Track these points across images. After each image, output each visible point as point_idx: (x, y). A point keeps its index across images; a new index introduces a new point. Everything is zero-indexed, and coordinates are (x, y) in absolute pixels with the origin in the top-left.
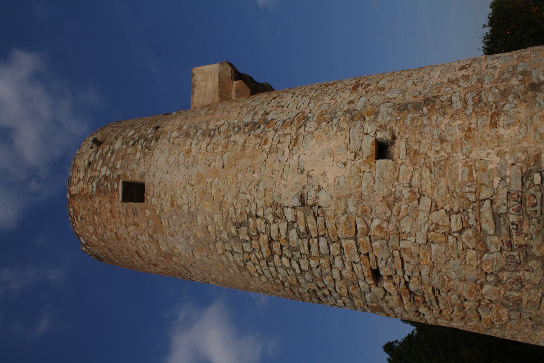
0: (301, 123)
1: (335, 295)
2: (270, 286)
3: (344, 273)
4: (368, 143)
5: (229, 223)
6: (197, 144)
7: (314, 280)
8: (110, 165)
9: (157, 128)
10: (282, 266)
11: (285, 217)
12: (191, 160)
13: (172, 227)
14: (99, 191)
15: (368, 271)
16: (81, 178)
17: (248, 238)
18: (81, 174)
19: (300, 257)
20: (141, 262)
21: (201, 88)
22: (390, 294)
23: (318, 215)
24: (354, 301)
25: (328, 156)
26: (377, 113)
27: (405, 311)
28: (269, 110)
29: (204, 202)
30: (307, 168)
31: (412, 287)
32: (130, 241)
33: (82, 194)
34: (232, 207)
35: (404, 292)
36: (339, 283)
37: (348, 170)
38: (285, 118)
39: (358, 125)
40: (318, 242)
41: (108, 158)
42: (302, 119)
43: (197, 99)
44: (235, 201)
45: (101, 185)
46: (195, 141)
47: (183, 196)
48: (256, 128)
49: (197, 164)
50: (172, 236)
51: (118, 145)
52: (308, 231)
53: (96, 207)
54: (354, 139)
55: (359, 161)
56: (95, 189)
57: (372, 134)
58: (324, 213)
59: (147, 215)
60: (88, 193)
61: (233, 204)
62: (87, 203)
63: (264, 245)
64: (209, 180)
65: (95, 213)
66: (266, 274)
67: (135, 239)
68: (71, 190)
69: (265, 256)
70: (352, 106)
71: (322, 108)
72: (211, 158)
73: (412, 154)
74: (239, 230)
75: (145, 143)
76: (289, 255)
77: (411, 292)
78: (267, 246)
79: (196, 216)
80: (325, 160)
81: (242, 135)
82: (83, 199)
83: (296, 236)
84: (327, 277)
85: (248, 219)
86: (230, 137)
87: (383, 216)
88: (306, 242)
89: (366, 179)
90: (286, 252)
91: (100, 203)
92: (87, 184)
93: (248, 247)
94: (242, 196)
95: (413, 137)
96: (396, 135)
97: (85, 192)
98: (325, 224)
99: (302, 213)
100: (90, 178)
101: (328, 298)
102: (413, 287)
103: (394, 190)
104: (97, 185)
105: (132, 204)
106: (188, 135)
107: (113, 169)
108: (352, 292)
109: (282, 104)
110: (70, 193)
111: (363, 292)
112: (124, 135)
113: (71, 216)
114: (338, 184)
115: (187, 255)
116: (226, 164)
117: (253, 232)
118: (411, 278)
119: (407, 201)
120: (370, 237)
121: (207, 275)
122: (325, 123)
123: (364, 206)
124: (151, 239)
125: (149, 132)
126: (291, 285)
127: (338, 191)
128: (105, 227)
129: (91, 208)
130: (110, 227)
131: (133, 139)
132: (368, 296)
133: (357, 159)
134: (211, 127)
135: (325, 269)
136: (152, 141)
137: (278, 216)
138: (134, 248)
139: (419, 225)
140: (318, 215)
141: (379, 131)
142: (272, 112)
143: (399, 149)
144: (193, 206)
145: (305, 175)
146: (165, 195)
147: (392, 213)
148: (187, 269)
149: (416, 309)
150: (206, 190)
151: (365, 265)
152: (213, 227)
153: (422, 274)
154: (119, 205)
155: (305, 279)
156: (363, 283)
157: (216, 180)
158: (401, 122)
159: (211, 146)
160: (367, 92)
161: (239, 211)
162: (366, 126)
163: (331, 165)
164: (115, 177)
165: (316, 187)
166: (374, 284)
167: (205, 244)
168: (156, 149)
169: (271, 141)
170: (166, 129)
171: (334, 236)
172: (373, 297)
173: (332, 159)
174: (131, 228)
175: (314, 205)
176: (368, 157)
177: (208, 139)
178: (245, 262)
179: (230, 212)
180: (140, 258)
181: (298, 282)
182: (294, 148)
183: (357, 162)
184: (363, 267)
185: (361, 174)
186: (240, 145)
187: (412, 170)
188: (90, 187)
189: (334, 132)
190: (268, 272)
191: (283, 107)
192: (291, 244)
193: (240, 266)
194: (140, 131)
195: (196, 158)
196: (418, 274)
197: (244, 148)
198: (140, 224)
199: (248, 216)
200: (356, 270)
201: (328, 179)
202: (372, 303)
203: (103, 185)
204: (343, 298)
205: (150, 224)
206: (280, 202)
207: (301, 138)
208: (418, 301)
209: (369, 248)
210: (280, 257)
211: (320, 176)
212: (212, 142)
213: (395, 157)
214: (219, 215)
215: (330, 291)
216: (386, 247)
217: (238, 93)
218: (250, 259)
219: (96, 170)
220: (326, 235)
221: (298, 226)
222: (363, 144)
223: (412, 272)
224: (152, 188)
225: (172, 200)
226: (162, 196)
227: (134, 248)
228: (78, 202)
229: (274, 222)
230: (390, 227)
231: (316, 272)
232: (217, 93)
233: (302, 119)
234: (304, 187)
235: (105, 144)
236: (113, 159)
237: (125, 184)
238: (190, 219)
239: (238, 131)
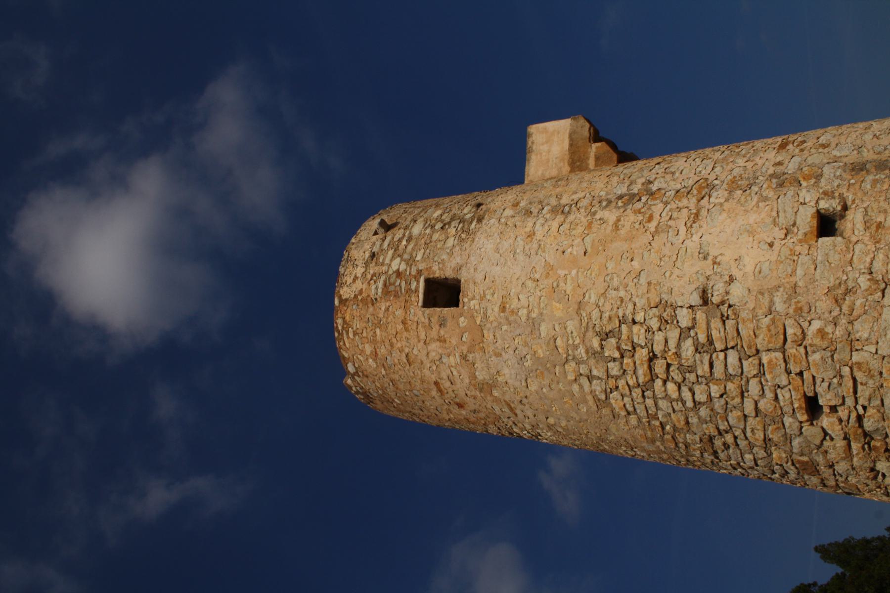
0: (703, 193)
1: (742, 443)
2: (641, 432)
3: (762, 405)
4: (806, 215)
5: (590, 333)
6: (543, 225)
7: (714, 419)
8: (406, 256)
9: (479, 205)
10: (667, 396)
11: (678, 322)
12: (535, 246)
13: (500, 341)
14: (386, 292)
15: (799, 400)
16: (359, 275)
17: (617, 355)
18: (359, 271)
19: (695, 381)
20: (439, 401)
21: (541, 154)
22: (832, 439)
23: (727, 318)
24: (771, 453)
25: (745, 235)
26: (818, 177)
27: (853, 469)
28: (654, 177)
29: (554, 303)
30: (713, 252)
31: (868, 425)
32: (428, 365)
33: (360, 298)
34: (597, 309)
35: (855, 434)
36: (751, 422)
37: (776, 252)
38: (679, 186)
39: (790, 193)
40: (726, 358)
41: (402, 246)
42: (705, 188)
43: (534, 169)
44: (602, 300)
45: (391, 284)
46: (541, 221)
47: (521, 297)
48: (635, 200)
49: (544, 252)
50: (498, 355)
51: (417, 229)
52: (711, 342)
53: (381, 315)
54: (785, 211)
55: (792, 240)
56: (380, 291)
57: (813, 204)
58: (737, 315)
59: (461, 325)
60: (369, 296)
61: (597, 306)
62: (367, 311)
63: (642, 364)
64: (562, 273)
65: (378, 324)
66: (638, 411)
67: (437, 363)
68: (342, 292)
69: (641, 381)
70: (779, 169)
71: (735, 173)
72: (566, 242)
73: (874, 228)
74: (603, 343)
75: (461, 225)
76: (679, 378)
77: (866, 434)
78: (646, 366)
79: (539, 325)
80: (740, 240)
81: (614, 210)
82: (361, 305)
83: (692, 349)
84: (734, 412)
85: (620, 326)
86: (595, 213)
87: (827, 315)
88: (706, 358)
89: (802, 264)
90: (675, 374)
91: (387, 309)
92: (369, 283)
93: (616, 369)
94: (612, 293)
95: (875, 206)
96: (849, 203)
97: (364, 295)
98: (738, 330)
99: (704, 315)
100: (374, 275)
101: (731, 451)
102: (870, 423)
103: (845, 278)
104: (385, 285)
105: (438, 309)
106: (528, 213)
107: (411, 262)
108: (771, 436)
109: (672, 170)
110: (340, 297)
111: (788, 436)
112: (425, 216)
113: (338, 331)
114: (760, 272)
115: (517, 384)
116: (589, 250)
117: (626, 345)
118: (868, 409)
119: (866, 294)
120: (805, 348)
121: (542, 417)
122: (739, 192)
123: (798, 302)
124: (463, 361)
125: (465, 211)
126: (675, 428)
127: (759, 282)
128: (392, 345)
129: (371, 318)
130: (399, 345)
131: (442, 221)
132: (796, 442)
133: (788, 238)
134: (564, 201)
135: (733, 399)
136: (471, 222)
137: (666, 321)
138: (433, 376)
139: (883, 327)
140: (727, 318)
141: (823, 199)
142: (657, 180)
143: (853, 222)
144: (536, 310)
145: (710, 261)
146: (493, 295)
147: (841, 310)
148: (511, 409)
149: (872, 465)
150: (558, 286)
151: (796, 389)
152: (565, 340)
153: (885, 404)
154: (418, 312)
155: (699, 418)
156: (791, 420)
157: (574, 272)
158: (857, 186)
159: (566, 226)
160: (802, 150)
161: (606, 315)
162: (803, 193)
163: (749, 247)
164: (414, 272)
165: (727, 278)
166: (807, 421)
167: (548, 365)
168: (478, 234)
169: (658, 217)
170: (492, 206)
171: (750, 347)
172: (804, 445)
173: (751, 239)
174: (434, 346)
175: (723, 303)
176: (806, 234)
177: (560, 218)
178: (607, 393)
179: (594, 318)
180: (439, 394)
181: (687, 423)
182: (694, 225)
183: (789, 241)
184: (793, 393)
185: (796, 258)
186: (611, 224)
187: (874, 249)
188: (373, 287)
189: (754, 203)
190: (643, 407)
191: (673, 173)
192: (683, 361)
193: (599, 400)
194: (451, 210)
195: (542, 243)
196: (878, 402)
197: (616, 226)
198: (448, 340)
199: (620, 321)
200: (780, 397)
201: (744, 266)
202: (802, 455)
203: (394, 284)
204: (755, 450)
205: (464, 339)
206: (671, 300)
207: (704, 213)
208: (876, 448)
209: (804, 363)
210: (665, 382)
211: (732, 262)
212: (568, 221)
213: (847, 233)
214: (577, 322)
215: (735, 438)
216: (829, 361)
217: (600, 160)
218: (617, 387)
219: (382, 264)
220: (739, 347)
221: (697, 334)
222: (798, 217)
223: (870, 400)
224: (471, 286)
225: (502, 302)
226: (488, 297)
227: (433, 376)
228: (352, 310)
229: (660, 329)
230: (837, 332)
231: (718, 405)
232: (566, 162)
233: (704, 188)
234: (708, 278)
235: (396, 228)
236: (410, 247)
237: (428, 281)
238: (529, 329)
239: (607, 206)
